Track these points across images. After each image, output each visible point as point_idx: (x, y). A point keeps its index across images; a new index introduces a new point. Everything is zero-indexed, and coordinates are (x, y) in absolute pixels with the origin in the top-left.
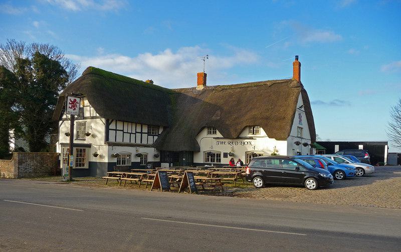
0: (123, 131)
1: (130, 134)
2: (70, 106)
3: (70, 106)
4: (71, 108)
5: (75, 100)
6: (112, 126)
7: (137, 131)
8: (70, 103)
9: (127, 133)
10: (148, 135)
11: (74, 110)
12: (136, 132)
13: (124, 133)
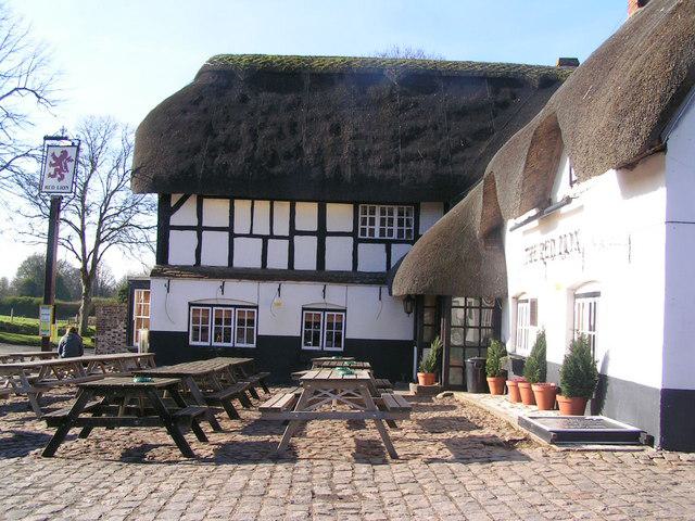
0: (230, 229)
1: (265, 239)
2: (52, 170)
6: (185, 215)
7: (298, 227)
9: (251, 235)
10: (357, 242)
11: (59, 180)
12: (293, 232)
13: (232, 236)
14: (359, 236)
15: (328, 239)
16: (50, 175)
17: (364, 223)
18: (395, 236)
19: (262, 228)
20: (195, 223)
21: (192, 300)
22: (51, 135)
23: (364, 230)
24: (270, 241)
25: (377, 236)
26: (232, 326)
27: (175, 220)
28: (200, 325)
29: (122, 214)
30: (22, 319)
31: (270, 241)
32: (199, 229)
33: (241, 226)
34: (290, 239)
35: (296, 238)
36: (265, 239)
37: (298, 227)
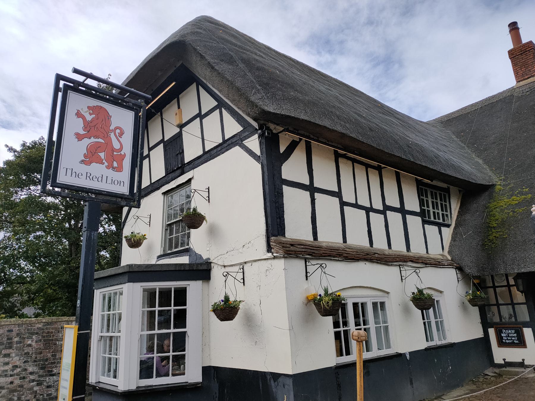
0: (338, 194)
13: (343, 204)
15: (316, 185)
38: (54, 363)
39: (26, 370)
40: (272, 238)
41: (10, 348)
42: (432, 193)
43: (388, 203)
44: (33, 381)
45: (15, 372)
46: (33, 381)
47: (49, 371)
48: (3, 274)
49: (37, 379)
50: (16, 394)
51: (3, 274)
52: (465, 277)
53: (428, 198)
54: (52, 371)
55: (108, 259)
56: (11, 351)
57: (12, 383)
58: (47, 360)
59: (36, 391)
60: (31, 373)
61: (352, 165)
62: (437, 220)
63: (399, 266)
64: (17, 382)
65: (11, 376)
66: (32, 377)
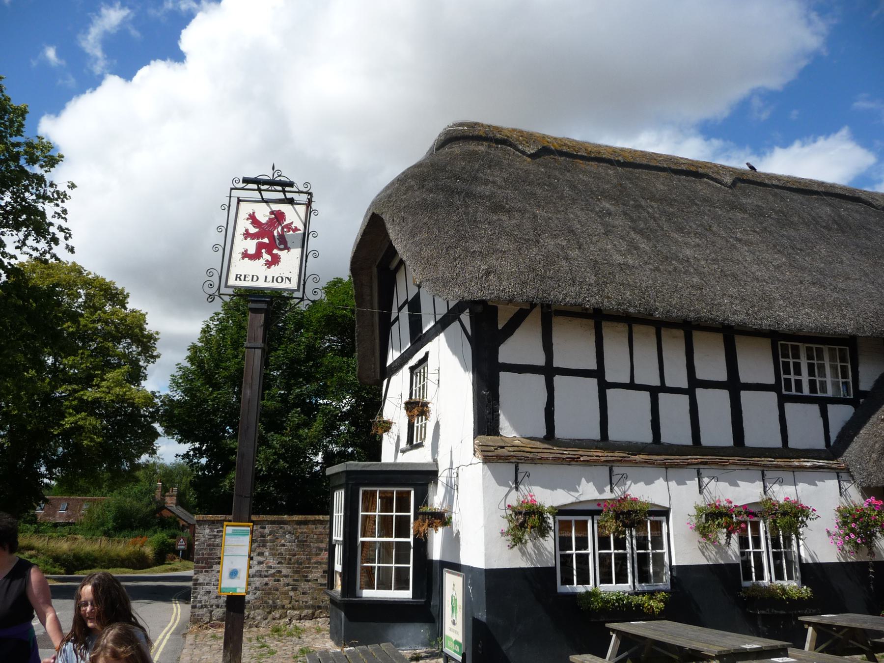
0: (599, 373)
1: (654, 392)
2: (251, 246)
3: (251, 246)
4: (252, 257)
5: (279, 217)
8: (247, 235)
9: (632, 386)
10: (782, 400)
11: (269, 264)
13: (604, 386)
14: (784, 392)
15: (540, 379)
16: (245, 255)
17: (787, 372)
18: (830, 393)
19: (648, 375)
20: (540, 361)
21: (420, 449)
22: (252, 175)
23: (788, 381)
24: (661, 396)
25: (806, 391)
26: (629, 550)
27: (507, 353)
28: (815, 362)
29: (490, 416)
30: (295, 516)
31: (661, 396)
32: (549, 372)
33: (616, 372)
34: (690, 392)
35: (700, 392)
36: (654, 392)
37: (685, 399)
38: (309, 567)
39: (280, 572)
40: (388, 455)
41: (264, 546)
42: (809, 350)
43: (700, 375)
44: (288, 585)
45: (270, 572)
46: (288, 585)
47: (304, 576)
48: (126, 405)
49: (292, 583)
50: (271, 596)
51: (126, 405)
52: (611, 484)
53: (799, 358)
54: (307, 576)
55: (608, 182)
56: (264, 549)
57: (266, 584)
58: (301, 563)
59: (291, 597)
60: (286, 576)
61: (627, 335)
62: (819, 394)
63: (793, 472)
64: (271, 583)
65: (266, 576)
66: (286, 580)
